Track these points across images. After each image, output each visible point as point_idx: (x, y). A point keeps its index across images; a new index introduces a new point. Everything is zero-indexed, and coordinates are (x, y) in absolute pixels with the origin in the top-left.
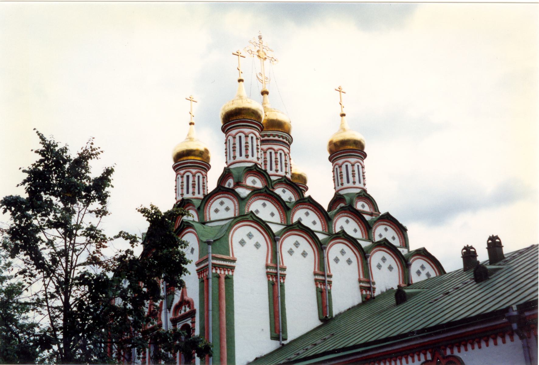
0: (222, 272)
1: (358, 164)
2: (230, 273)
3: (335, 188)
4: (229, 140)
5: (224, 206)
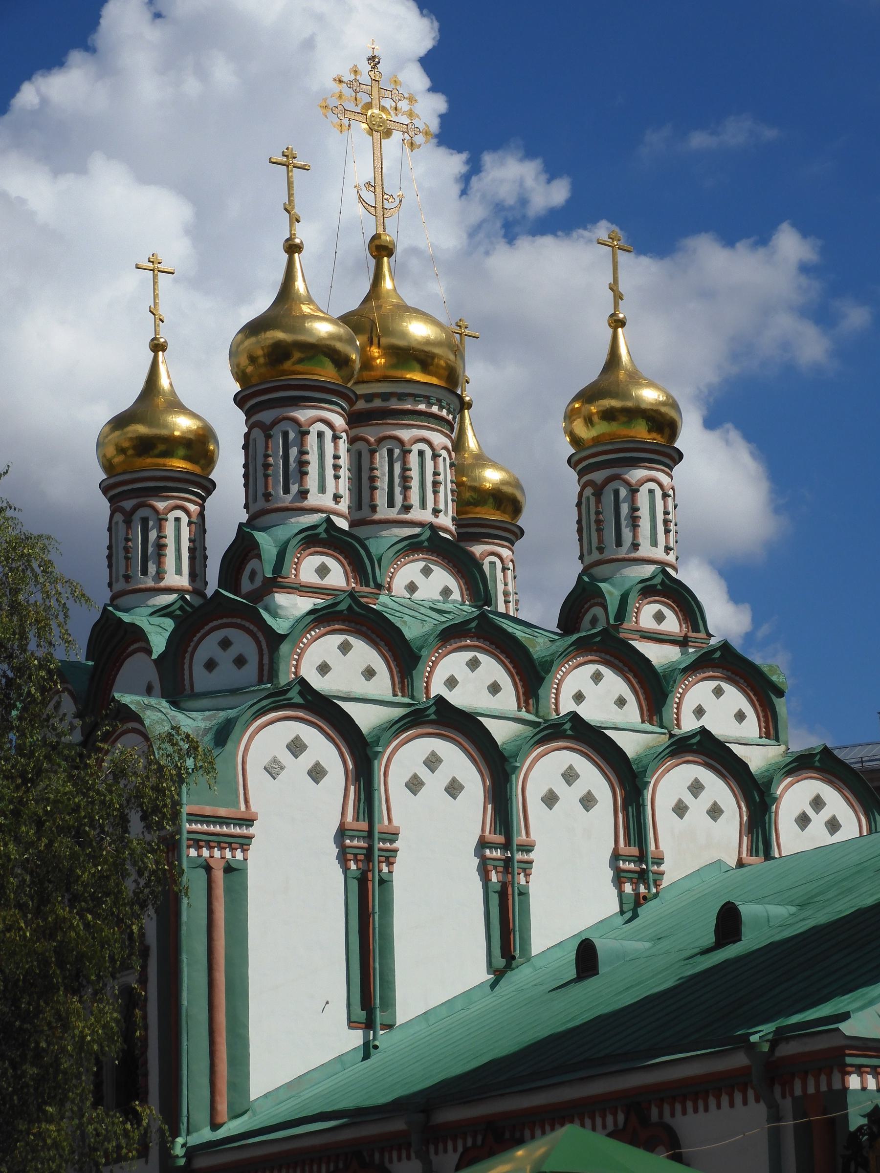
0: (217, 853)
1: (653, 485)
2: (239, 855)
3: (581, 558)
4: (255, 440)
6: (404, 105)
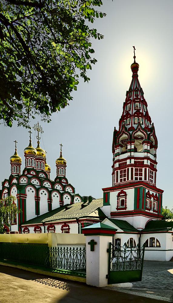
5: (24, 180)
6: (41, 129)
